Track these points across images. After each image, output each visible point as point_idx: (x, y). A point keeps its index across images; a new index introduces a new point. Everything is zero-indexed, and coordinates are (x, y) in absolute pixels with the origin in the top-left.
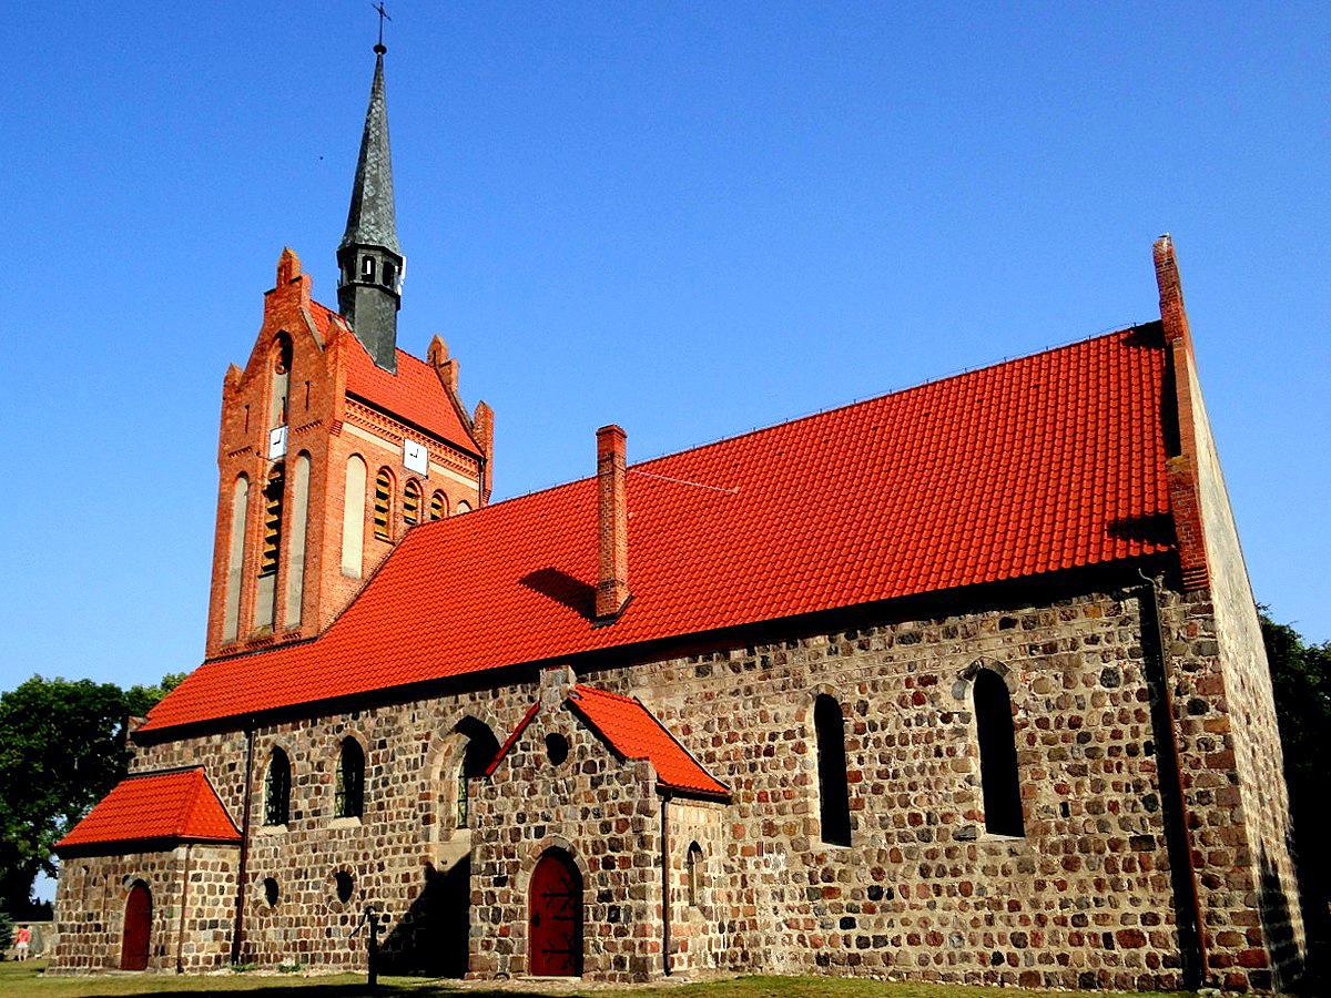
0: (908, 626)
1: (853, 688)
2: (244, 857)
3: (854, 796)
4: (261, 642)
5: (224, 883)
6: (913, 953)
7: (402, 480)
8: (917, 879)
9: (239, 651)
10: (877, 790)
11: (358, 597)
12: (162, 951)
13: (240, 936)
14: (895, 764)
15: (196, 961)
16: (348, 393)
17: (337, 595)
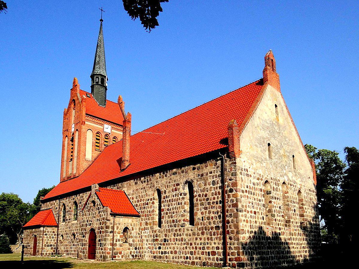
0: (175, 170)
1: (164, 187)
2: (58, 230)
3: (162, 215)
4: (69, 178)
5: (53, 236)
6: (171, 255)
7: (103, 135)
8: (173, 237)
9: (66, 180)
10: (167, 213)
11: (90, 166)
12: (38, 252)
13: (57, 248)
14: (171, 207)
15: (46, 254)
16: (86, 114)
17: (85, 165)
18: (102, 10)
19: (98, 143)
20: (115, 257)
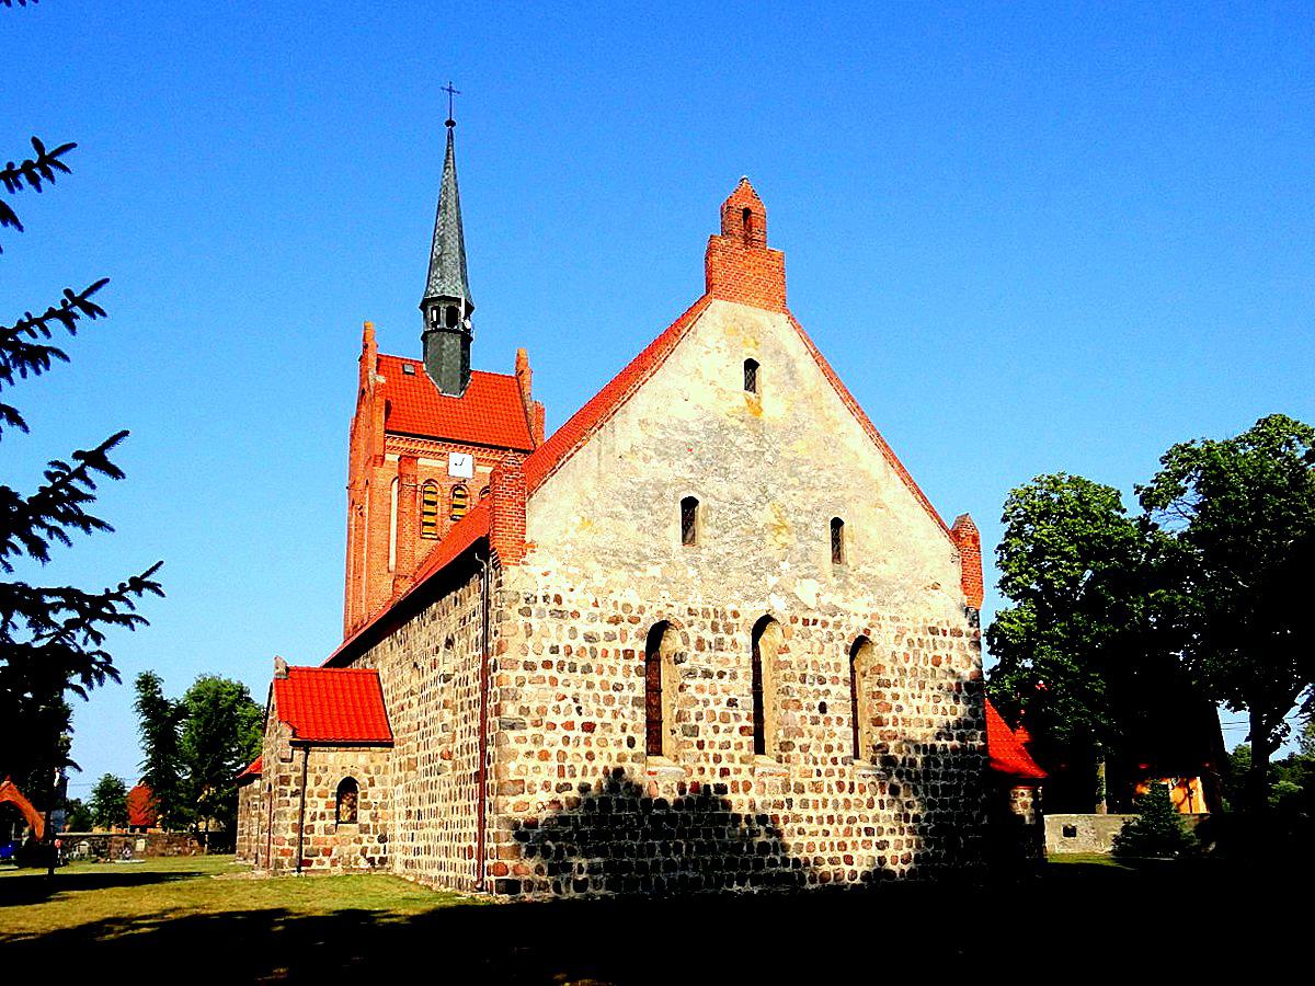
7: (447, 486)
18: (450, 90)
19: (433, 514)
20: (309, 863)
